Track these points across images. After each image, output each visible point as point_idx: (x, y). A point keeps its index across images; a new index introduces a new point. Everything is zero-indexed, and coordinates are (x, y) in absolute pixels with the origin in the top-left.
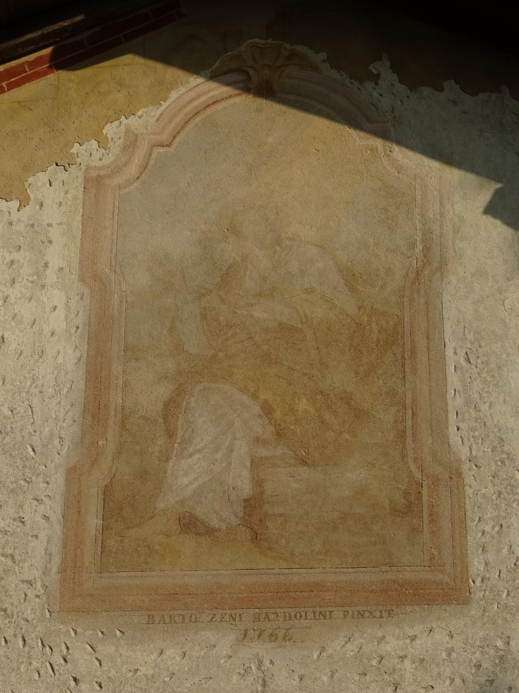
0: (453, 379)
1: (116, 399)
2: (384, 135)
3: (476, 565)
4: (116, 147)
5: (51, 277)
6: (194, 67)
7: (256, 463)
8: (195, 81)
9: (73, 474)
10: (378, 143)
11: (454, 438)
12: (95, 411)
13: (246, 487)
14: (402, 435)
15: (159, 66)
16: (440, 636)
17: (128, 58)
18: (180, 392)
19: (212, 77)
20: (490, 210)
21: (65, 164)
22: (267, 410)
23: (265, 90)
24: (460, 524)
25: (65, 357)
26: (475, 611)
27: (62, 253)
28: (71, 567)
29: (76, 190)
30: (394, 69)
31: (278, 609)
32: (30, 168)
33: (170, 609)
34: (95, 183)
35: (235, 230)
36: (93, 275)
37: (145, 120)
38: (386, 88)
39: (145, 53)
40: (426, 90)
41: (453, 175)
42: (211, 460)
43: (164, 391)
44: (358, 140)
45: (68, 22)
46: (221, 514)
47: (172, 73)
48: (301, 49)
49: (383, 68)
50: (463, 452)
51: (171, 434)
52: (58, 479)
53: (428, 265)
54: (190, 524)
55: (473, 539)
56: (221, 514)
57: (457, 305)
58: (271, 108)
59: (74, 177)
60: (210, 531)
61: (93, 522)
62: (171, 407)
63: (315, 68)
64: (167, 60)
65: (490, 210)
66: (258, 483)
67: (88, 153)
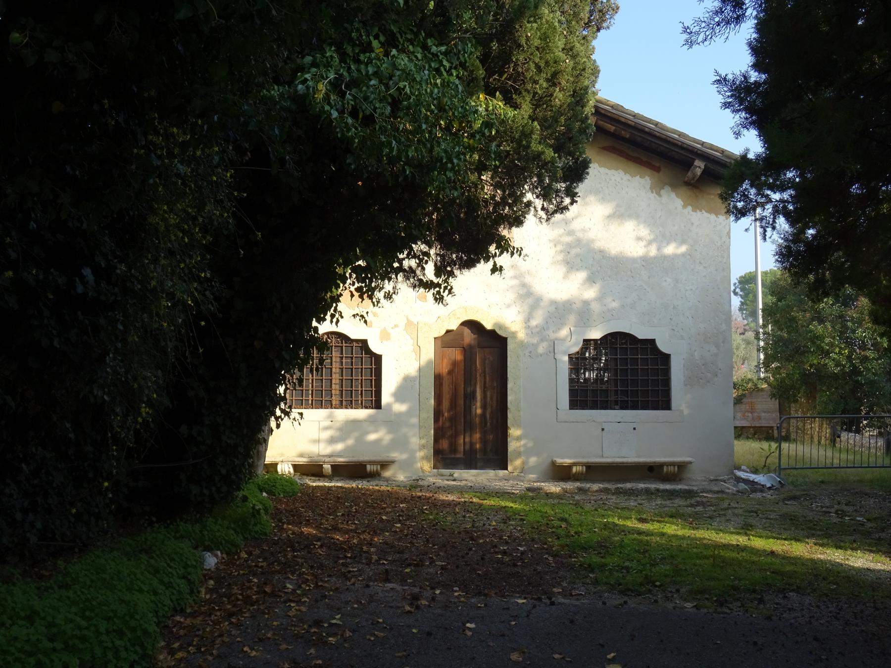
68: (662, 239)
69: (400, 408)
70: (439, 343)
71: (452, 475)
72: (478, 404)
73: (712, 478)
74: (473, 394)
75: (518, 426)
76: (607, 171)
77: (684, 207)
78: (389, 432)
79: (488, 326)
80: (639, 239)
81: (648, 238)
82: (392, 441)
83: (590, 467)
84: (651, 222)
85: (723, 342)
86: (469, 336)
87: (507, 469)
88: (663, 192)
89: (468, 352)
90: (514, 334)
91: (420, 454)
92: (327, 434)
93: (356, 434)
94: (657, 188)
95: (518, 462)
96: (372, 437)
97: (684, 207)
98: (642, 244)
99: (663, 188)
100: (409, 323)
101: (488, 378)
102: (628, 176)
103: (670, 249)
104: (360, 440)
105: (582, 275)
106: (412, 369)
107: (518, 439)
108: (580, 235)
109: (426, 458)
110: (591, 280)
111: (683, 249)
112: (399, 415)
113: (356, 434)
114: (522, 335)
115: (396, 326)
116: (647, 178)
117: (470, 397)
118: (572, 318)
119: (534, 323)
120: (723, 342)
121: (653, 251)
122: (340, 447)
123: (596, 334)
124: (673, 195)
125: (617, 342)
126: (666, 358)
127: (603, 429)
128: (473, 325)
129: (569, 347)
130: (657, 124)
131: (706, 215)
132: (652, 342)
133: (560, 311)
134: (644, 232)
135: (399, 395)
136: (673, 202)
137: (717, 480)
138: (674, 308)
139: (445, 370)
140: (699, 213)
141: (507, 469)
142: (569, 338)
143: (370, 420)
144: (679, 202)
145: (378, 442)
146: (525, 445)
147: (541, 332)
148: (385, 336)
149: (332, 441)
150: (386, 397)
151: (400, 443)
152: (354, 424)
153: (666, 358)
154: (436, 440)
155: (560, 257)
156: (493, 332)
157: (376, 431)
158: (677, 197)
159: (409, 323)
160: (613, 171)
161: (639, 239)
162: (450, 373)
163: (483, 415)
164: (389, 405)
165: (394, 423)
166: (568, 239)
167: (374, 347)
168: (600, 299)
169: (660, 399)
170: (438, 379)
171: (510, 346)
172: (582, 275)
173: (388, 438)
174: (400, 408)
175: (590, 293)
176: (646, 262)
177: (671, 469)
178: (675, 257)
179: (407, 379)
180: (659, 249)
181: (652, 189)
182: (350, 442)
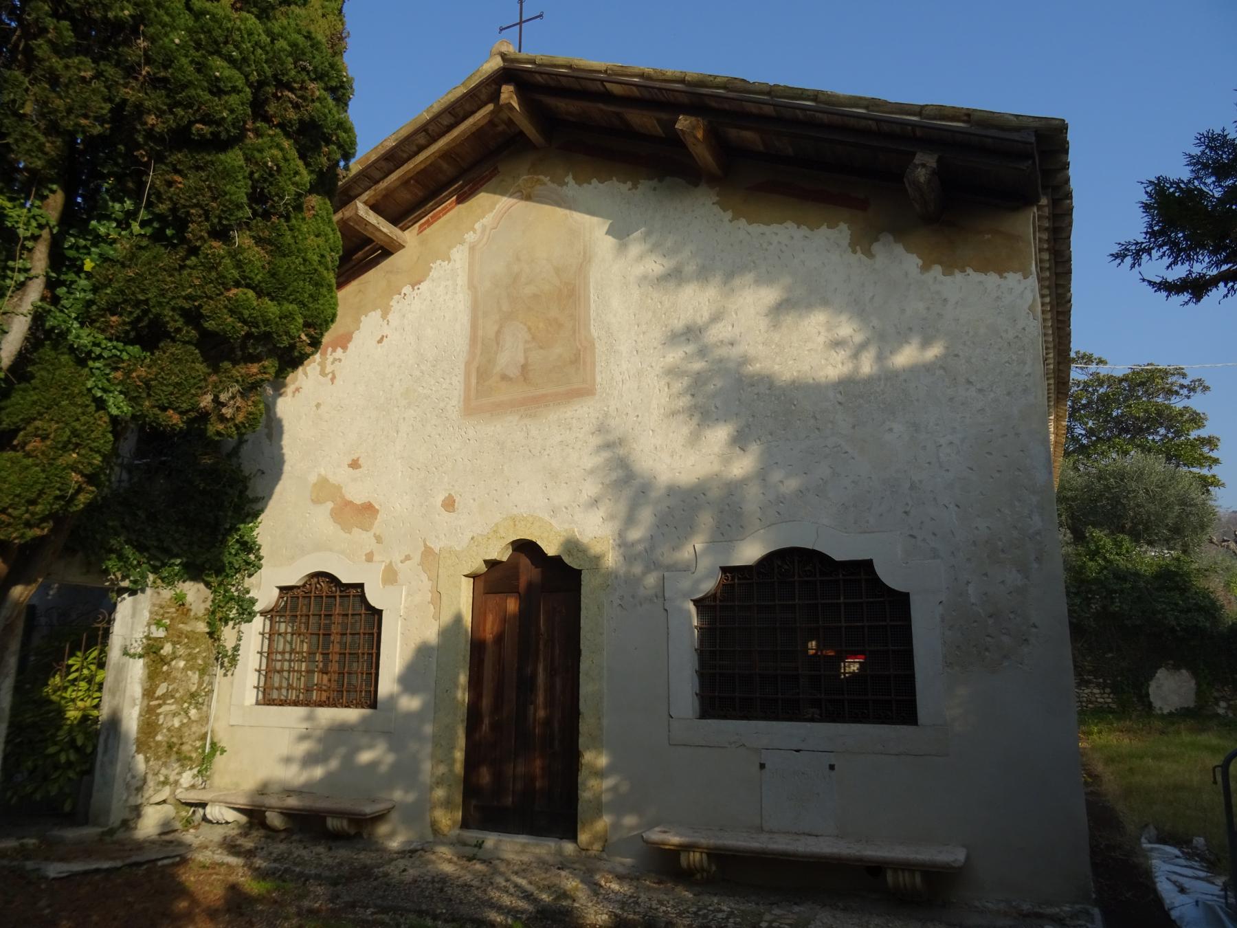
0: (593, 306)
1: (480, 333)
2: (570, 208)
3: (598, 379)
4: (479, 231)
5: (459, 288)
6: (503, 193)
7: (526, 351)
8: (505, 199)
9: (468, 364)
10: (567, 212)
11: (593, 330)
12: (473, 340)
13: (522, 361)
14: (574, 332)
15: (491, 195)
16: (585, 409)
17: (482, 194)
18: (501, 327)
19: (510, 196)
20: (608, 233)
21: (462, 242)
22: (529, 329)
23: (528, 198)
24: (594, 364)
25: (464, 319)
26: (597, 397)
27: (462, 280)
28: (467, 399)
29: (466, 254)
30: (574, 178)
31: (532, 405)
32: (450, 248)
33: (497, 410)
34: (472, 248)
35: (518, 259)
36: (472, 286)
37: (488, 219)
38: (571, 188)
39: (487, 191)
40: (585, 185)
41: (595, 220)
42: (509, 357)
43: (496, 328)
44: (560, 212)
45: (40, 260)
46: (513, 372)
47: (497, 197)
48: (541, 177)
49: (569, 179)
50: (595, 335)
51: (498, 344)
52: (463, 367)
53: (586, 259)
54: (504, 377)
55: (598, 369)
56: (513, 372)
57: (594, 275)
58: (530, 204)
59: (466, 247)
60: (511, 379)
61: (474, 381)
62: (498, 333)
63: (545, 184)
64: (495, 193)
65: (608, 233)
66: (526, 358)
67: (470, 237)
68: (886, 340)
69: (410, 703)
70: (481, 584)
71: (479, 845)
72: (541, 699)
73: (1026, 907)
74: (534, 677)
75: (597, 744)
76: (763, 228)
77: (925, 268)
78: (392, 748)
79: (551, 550)
80: (837, 344)
81: (859, 338)
82: (396, 768)
83: (720, 856)
84: (858, 308)
85: (1038, 559)
86: (528, 572)
87: (573, 837)
88: (876, 247)
89: (529, 601)
90: (597, 559)
91: (440, 793)
92: (303, 748)
93: (342, 750)
94: (863, 241)
95: (604, 822)
96: (365, 757)
97: (925, 268)
98: (842, 354)
99: (877, 240)
100: (428, 552)
101: (557, 651)
102: (804, 231)
103: (906, 356)
104: (348, 759)
105: (720, 435)
106: (431, 633)
107: (600, 774)
108: (723, 352)
109: (447, 804)
110: (740, 441)
111: (934, 352)
112: (409, 715)
113: (342, 750)
114: (611, 560)
115: (408, 558)
116: (843, 226)
117: (526, 686)
118: (706, 520)
119: (635, 534)
120: (1038, 559)
121: (867, 366)
122: (318, 772)
123: (750, 552)
124: (899, 249)
125: (792, 568)
126: (901, 601)
127: (762, 766)
128: (525, 548)
129: (698, 582)
130: (815, 96)
131: (974, 276)
132: (866, 566)
133: (683, 507)
134: (847, 329)
135: (409, 680)
136: (900, 263)
137: (1040, 916)
138: (912, 487)
139: (490, 630)
140: (959, 276)
141: (573, 837)
142: (699, 561)
143: (365, 727)
144: (912, 262)
145: (373, 765)
146: (614, 789)
147: (644, 555)
148: (390, 576)
149: (310, 760)
150: (387, 684)
151: (404, 772)
152: (339, 732)
153: (898, 604)
154: (471, 763)
155: (685, 401)
156: (557, 560)
157: (370, 747)
158: (908, 249)
159: (428, 552)
160: (775, 227)
161: (837, 344)
162: (499, 638)
163: (548, 722)
164: (392, 699)
165: (395, 731)
166: (698, 365)
167: (373, 598)
168: (762, 475)
169: (888, 696)
170: (477, 647)
171: (588, 584)
172: (720, 435)
173: (390, 758)
174: (410, 703)
175: (742, 466)
176: (848, 387)
177: (904, 879)
178: (915, 370)
179: (423, 652)
180: (880, 358)
181: (853, 245)
182: (334, 764)
